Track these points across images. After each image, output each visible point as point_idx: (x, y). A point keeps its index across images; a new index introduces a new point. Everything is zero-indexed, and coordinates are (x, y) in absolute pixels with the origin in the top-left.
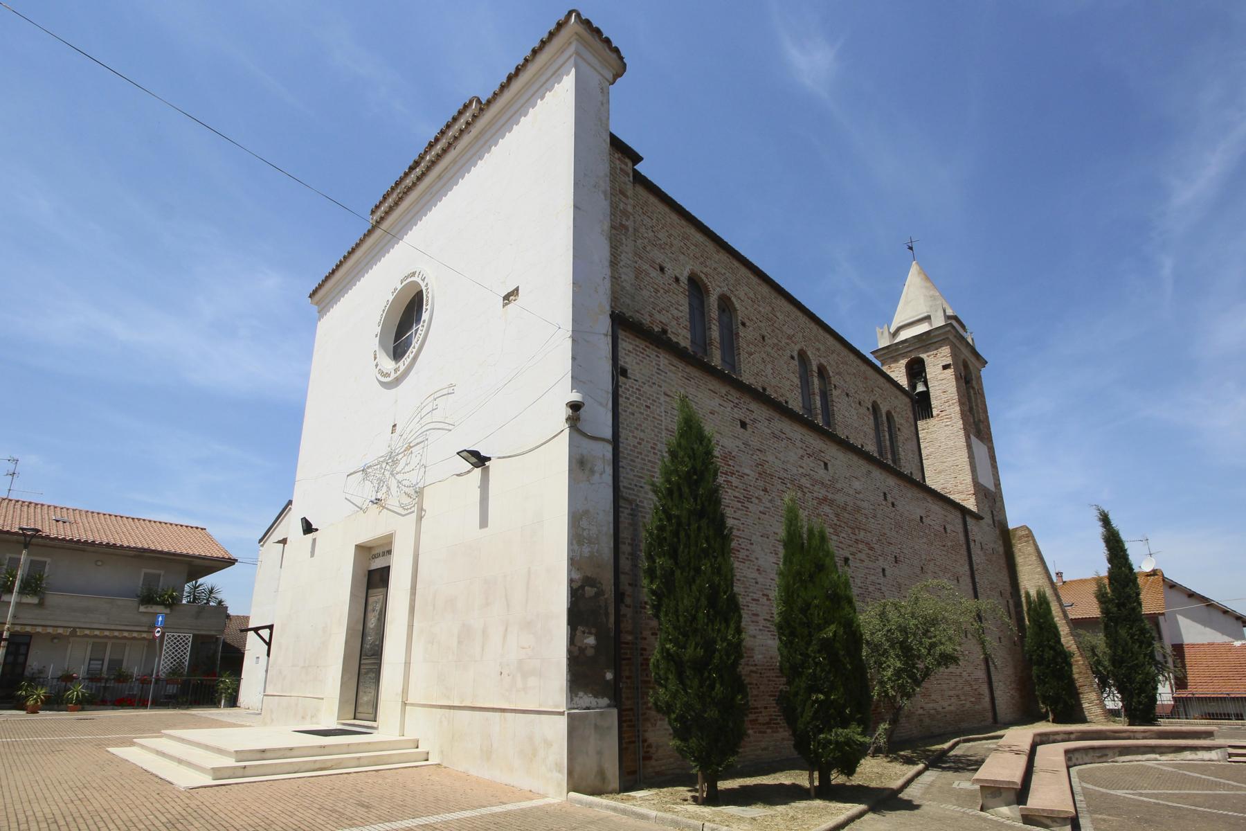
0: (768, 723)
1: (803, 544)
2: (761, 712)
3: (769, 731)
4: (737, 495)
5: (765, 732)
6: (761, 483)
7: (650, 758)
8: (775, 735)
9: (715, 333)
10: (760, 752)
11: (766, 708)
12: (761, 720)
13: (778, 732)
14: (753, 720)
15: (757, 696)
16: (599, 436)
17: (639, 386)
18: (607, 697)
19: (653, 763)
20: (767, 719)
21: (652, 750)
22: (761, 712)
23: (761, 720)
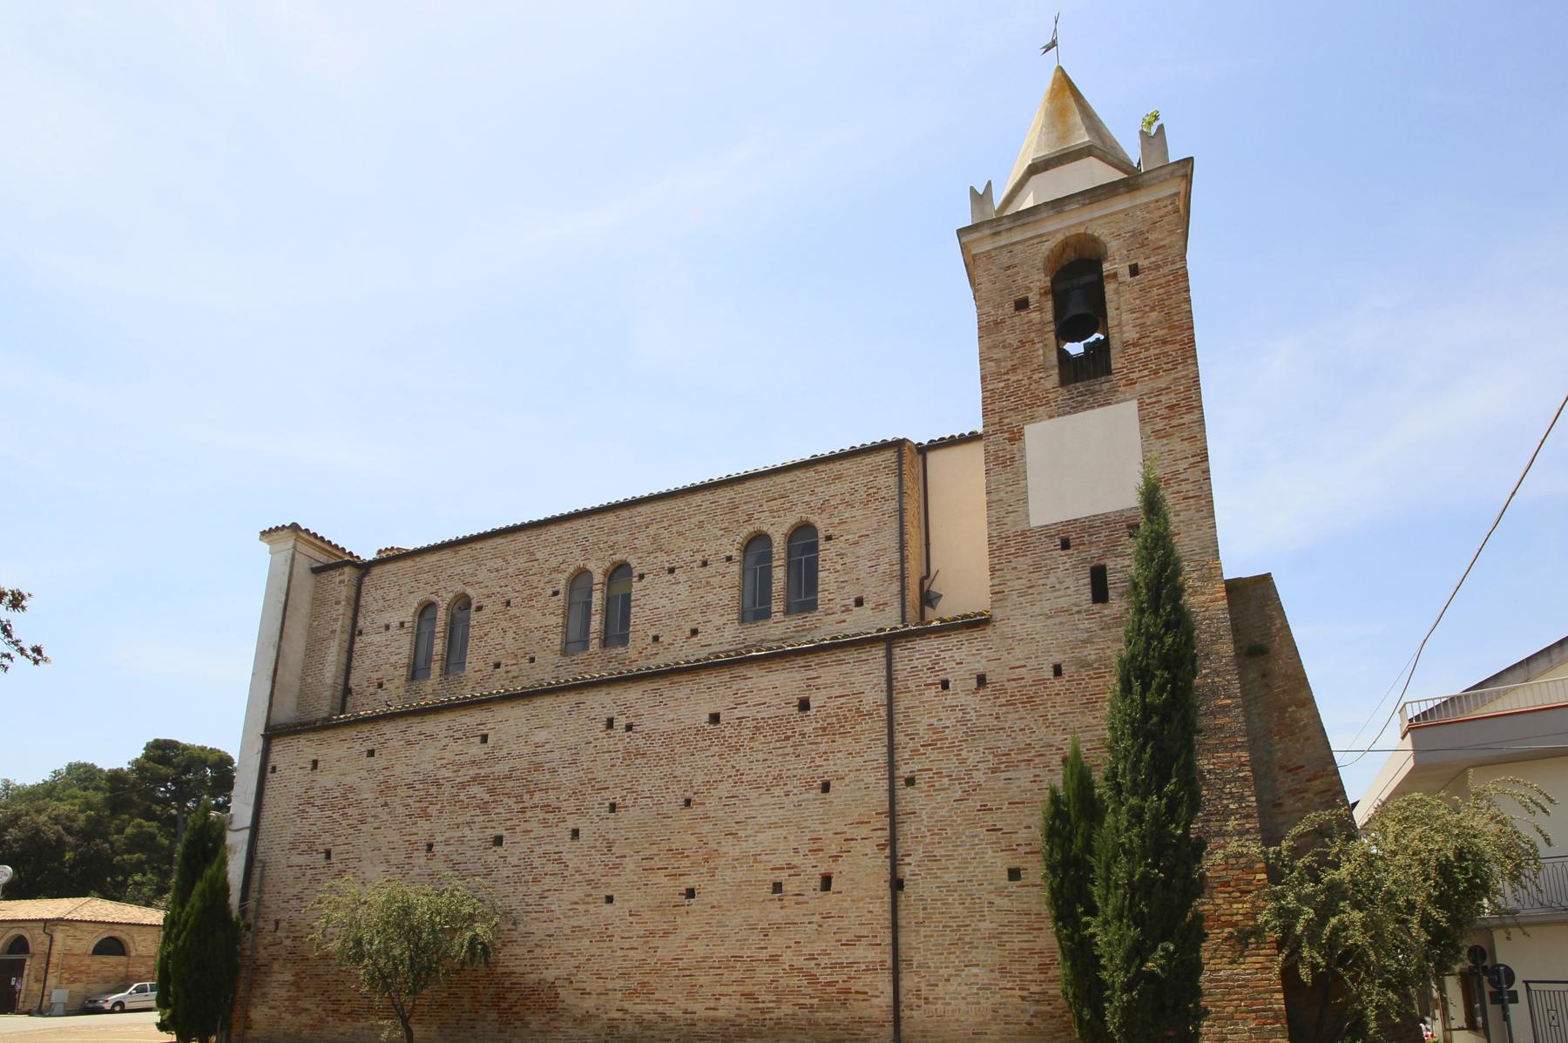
0: (349, 1013)
1: (1343, 1028)
2: (343, 1004)
3: (349, 1020)
4: (351, 822)
5: (344, 1021)
6: (381, 800)
7: (251, 1028)
8: (355, 1023)
9: (439, 646)
10: (337, 1036)
11: (350, 1001)
12: (342, 1010)
13: (359, 1022)
14: (335, 1010)
15: (342, 990)
16: (265, 714)
17: (698, 856)
18: (274, 739)
19: (252, 1031)
20: (349, 1010)
21: (253, 1023)
22: (343, 1004)
23: (342, 1010)
